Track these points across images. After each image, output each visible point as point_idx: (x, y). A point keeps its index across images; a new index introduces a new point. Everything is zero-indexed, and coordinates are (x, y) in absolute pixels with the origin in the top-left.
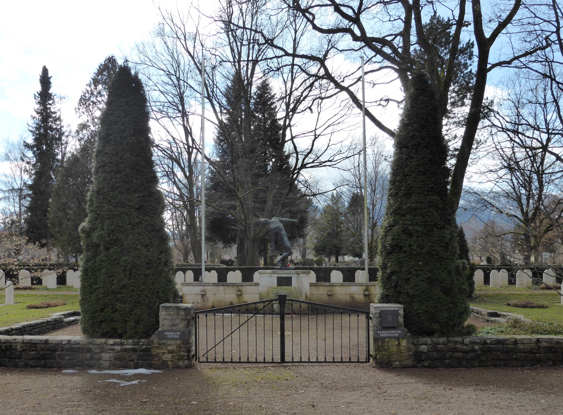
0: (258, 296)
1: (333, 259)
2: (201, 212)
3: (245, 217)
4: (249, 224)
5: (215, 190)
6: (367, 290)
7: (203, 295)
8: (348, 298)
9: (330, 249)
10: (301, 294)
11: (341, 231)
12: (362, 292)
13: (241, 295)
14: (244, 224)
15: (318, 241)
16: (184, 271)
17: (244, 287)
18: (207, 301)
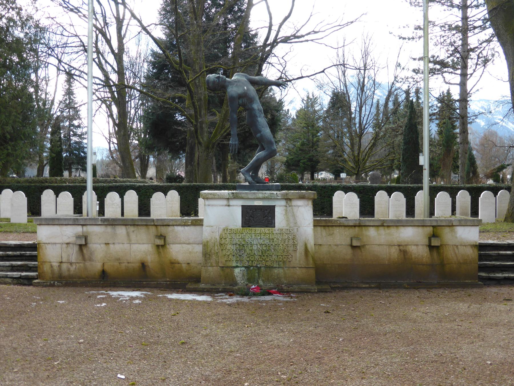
0: (199, 249)
1: (307, 176)
2: (135, 107)
3: (196, 112)
4: (202, 123)
5: (157, 78)
6: (434, 235)
7: (81, 246)
8: (394, 253)
9: (304, 163)
10: (295, 245)
11: (318, 141)
12: (426, 241)
13: (163, 246)
14: (194, 123)
15: (289, 154)
16: (122, 191)
17: (170, 228)
18: (91, 260)
